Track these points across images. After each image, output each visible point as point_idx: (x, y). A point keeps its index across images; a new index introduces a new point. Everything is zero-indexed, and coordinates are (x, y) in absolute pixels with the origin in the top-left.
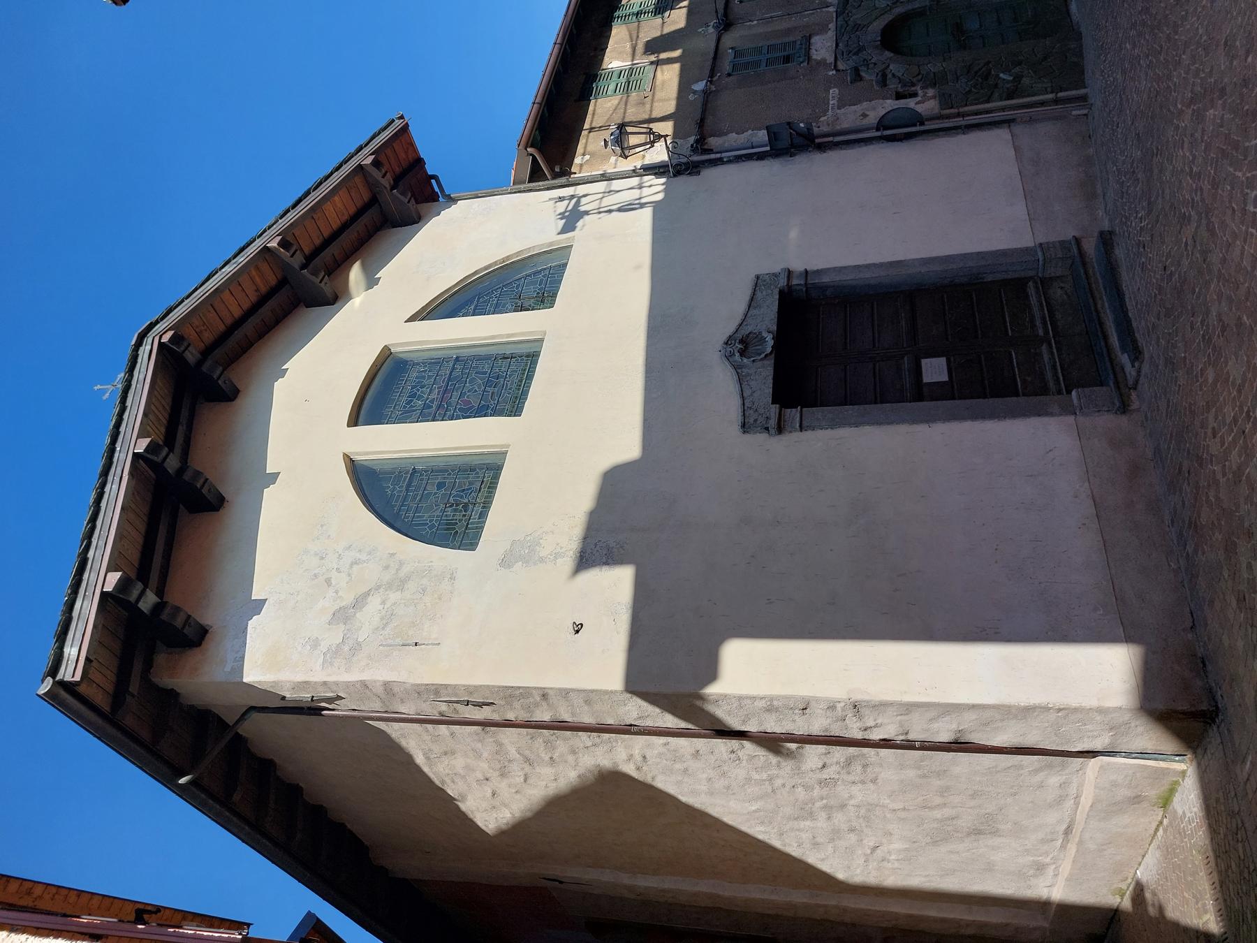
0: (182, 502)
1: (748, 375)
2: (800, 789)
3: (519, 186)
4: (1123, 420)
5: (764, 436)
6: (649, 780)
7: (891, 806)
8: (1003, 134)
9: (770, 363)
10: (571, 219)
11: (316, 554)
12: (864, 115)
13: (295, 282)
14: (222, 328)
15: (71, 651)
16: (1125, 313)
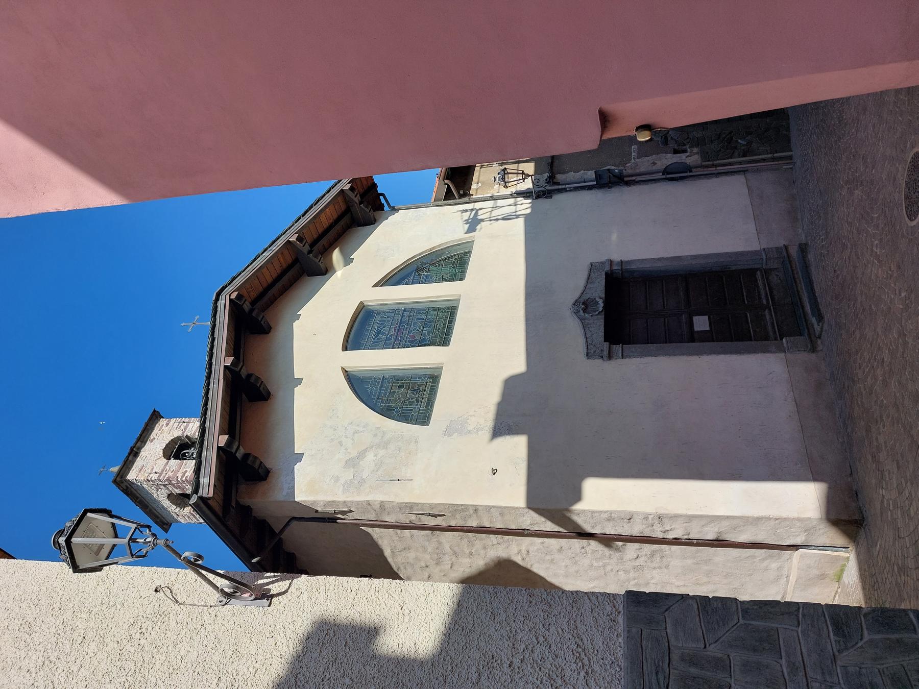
0: (250, 394)
1: (589, 324)
2: (621, 573)
3: (437, 203)
4: (813, 356)
5: (600, 361)
6: (529, 567)
7: (677, 584)
8: (739, 179)
9: (602, 317)
10: (473, 224)
11: (331, 427)
12: (654, 164)
13: (302, 263)
14: (261, 289)
15: (204, 480)
16: (814, 295)
